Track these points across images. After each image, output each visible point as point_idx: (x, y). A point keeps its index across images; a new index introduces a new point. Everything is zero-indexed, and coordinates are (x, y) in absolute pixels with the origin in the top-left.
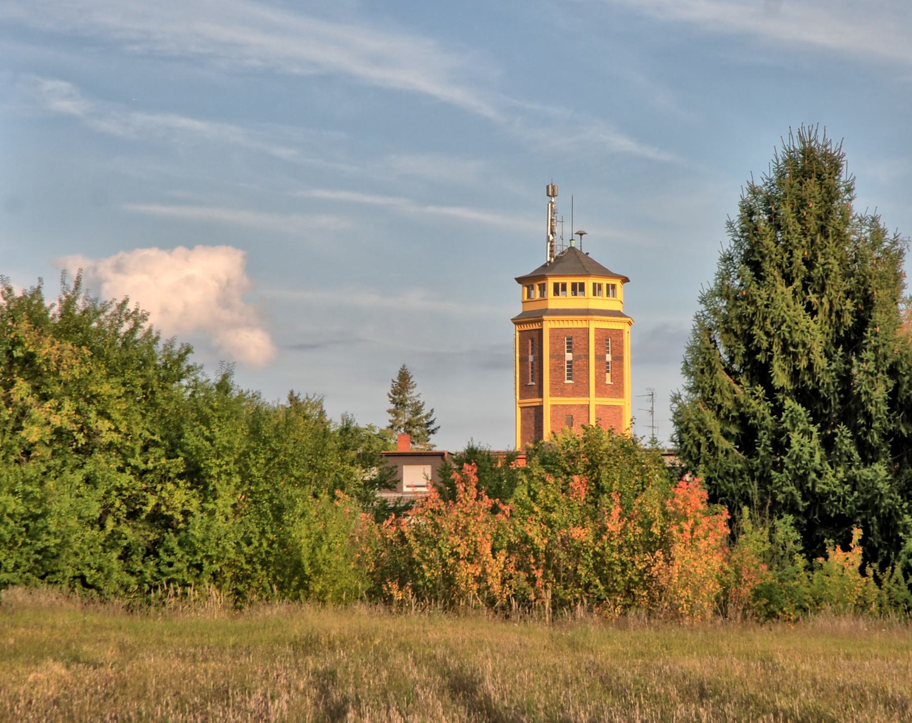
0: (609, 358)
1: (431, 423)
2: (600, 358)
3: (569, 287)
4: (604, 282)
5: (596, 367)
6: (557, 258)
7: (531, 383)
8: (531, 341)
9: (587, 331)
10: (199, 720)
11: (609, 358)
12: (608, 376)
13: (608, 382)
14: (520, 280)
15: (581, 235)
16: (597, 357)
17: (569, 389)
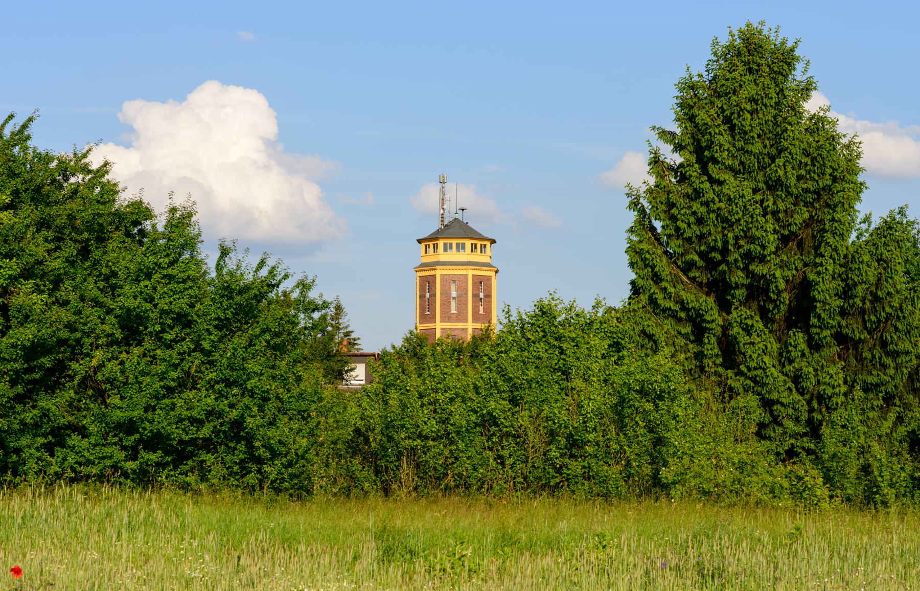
0: (482, 295)
2: (475, 296)
3: (454, 246)
4: (479, 243)
6: (447, 226)
9: (466, 276)
11: (482, 295)
17: (454, 317)
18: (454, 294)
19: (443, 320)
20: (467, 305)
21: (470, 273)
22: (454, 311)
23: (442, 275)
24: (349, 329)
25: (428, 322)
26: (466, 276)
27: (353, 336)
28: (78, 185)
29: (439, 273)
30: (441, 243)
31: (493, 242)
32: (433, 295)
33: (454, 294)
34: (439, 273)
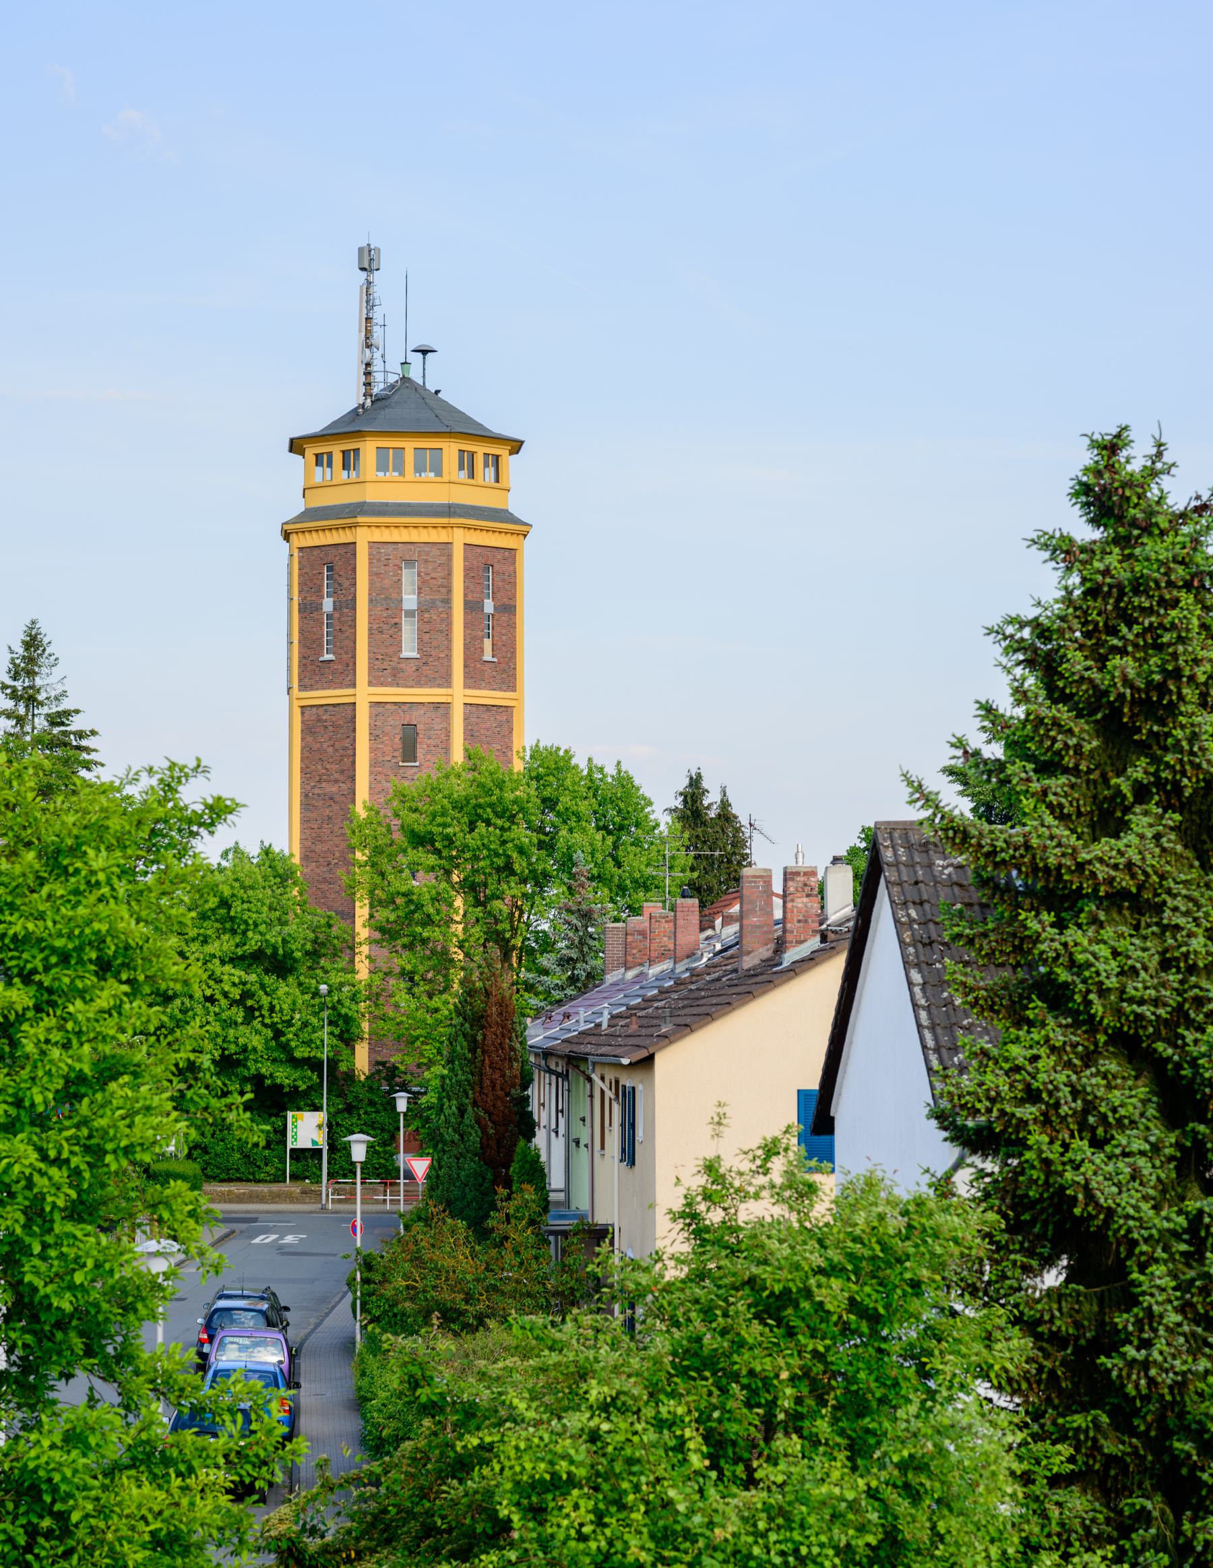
0: (489, 606)
1: (87, 750)
2: (473, 607)
3: (338, 459)
4: (480, 450)
5: (467, 626)
6: (378, 400)
7: (320, 652)
8: (322, 573)
9: (445, 548)
10: (21, 1151)
11: (489, 606)
12: (488, 643)
13: (488, 656)
14: (296, 446)
15: (425, 352)
16: (467, 604)
17: (410, 669)
18: (410, 601)
19: (375, 680)
20: (372, 619)
21: (459, 538)
22: (409, 650)
23: (372, 544)
24: (65, 705)
25: (330, 684)
26: (445, 548)
27: (76, 724)
28: (451, 905)
29: (363, 538)
30: (369, 449)
31: (516, 446)
32: (347, 605)
33: (410, 601)
34: (363, 538)
